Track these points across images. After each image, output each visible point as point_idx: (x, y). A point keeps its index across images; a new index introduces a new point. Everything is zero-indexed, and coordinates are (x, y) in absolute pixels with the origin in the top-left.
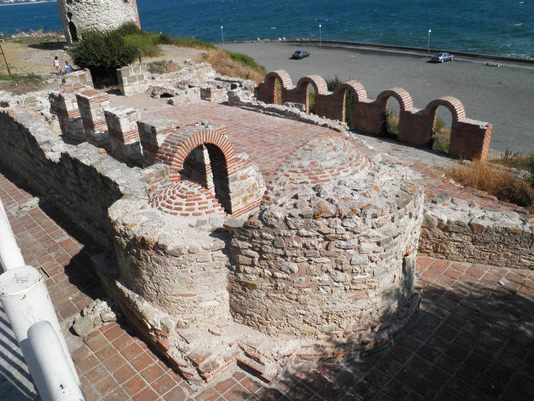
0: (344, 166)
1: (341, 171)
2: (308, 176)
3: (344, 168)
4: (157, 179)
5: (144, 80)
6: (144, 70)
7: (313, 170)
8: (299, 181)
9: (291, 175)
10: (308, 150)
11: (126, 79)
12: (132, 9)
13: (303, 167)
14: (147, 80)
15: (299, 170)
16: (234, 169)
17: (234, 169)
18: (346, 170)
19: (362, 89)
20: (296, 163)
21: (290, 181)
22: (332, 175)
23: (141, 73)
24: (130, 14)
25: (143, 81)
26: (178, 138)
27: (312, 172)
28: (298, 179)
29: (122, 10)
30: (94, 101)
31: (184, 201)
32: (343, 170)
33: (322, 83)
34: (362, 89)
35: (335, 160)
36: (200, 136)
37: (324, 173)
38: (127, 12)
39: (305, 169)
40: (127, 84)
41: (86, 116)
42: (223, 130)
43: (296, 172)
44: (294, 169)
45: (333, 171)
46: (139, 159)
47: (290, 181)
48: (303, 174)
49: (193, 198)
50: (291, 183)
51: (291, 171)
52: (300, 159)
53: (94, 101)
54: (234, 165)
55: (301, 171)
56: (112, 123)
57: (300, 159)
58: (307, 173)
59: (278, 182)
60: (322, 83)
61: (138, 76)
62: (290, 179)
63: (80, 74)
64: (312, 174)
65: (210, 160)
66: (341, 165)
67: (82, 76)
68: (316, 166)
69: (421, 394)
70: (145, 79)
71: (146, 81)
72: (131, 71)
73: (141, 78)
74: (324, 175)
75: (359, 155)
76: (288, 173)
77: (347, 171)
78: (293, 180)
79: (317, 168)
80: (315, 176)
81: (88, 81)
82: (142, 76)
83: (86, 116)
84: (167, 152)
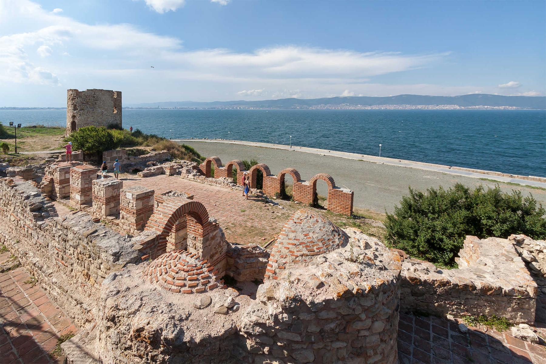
4: (148, 246)
8: (299, 254)
11: (109, 158)
12: (118, 116)
23: (121, 155)
24: (117, 119)
29: (112, 116)
38: (115, 118)
40: (109, 161)
51: (289, 244)
55: (299, 244)
62: (290, 251)
71: (124, 160)
72: (114, 154)
82: (122, 156)
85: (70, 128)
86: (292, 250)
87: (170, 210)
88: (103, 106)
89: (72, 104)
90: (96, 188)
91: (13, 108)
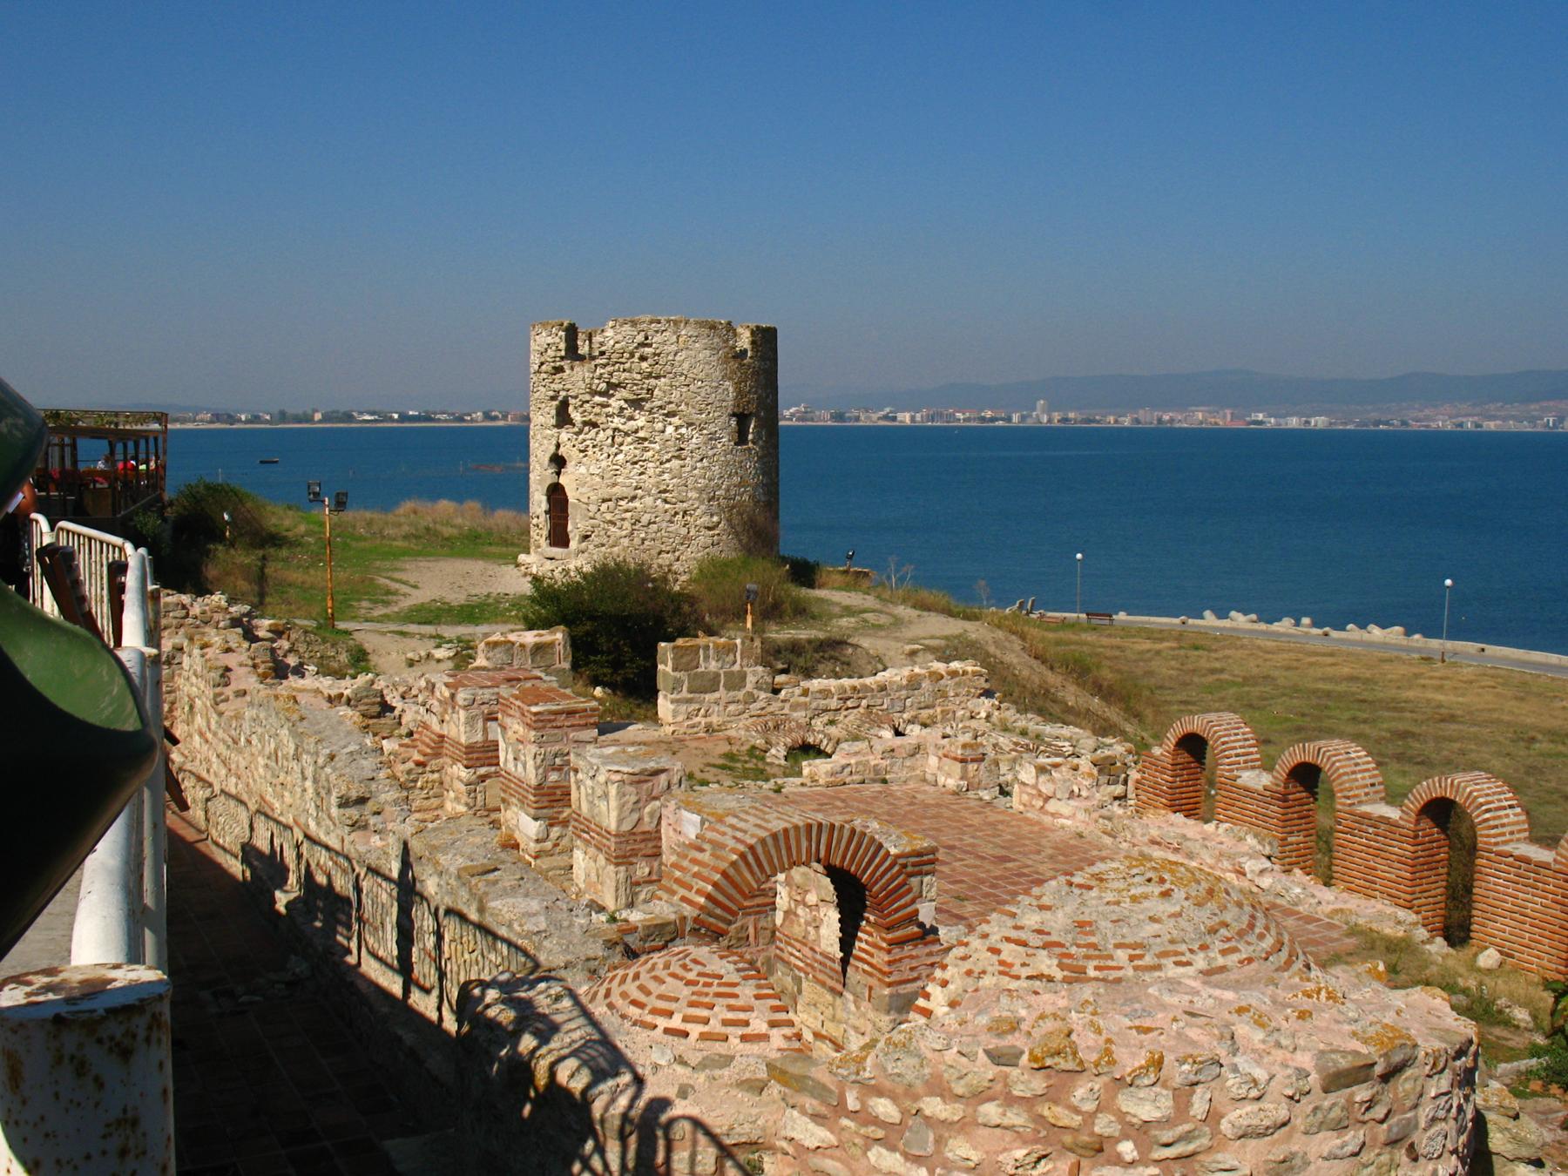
0: (1183, 948)
1: (1168, 962)
2: (1055, 962)
3: (1176, 953)
5: (744, 691)
6: (749, 658)
7: (1078, 946)
8: (1025, 972)
9: (1009, 952)
10: (1080, 886)
13: (1049, 934)
14: (755, 691)
15: (1036, 940)
16: (912, 969)
17: (912, 969)
18: (1184, 959)
19: (1511, 807)
20: (1032, 919)
21: (1001, 968)
22: (1136, 968)
23: (736, 667)
25: (740, 695)
26: (739, 835)
27: (1073, 950)
28: (1024, 965)
30: (550, 721)
31: (685, 992)
32: (1174, 959)
33: (1367, 770)
34: (1511, 807)
35: (1156, 926)
36: (809, 840)
37: (1111, 957)
39: (1054, 938)
41: (516, 766)
42: (925, 858)
43: (1024, 944)
44: (1022, 935)
45: (1141, 957)
46: (660, 949)
47: (1001, 968)
48: (1044, 953)
49: (715, 989)
50: (1001, 973)
51: (1008, 940)
52: (1048, 908)
53: (550, 721)
54: (912, 957)
56: (587, 795)
57: (1048, 908)
58: (1058, 950)
59: (967, 965)
60: (1367, 770)
61: (729, 675)
62: (1002, 963)
63: (537, 639)
64: (1070, 956)
65: (841, 930)
66: (1172, 942)
67: (539, 649)
68: (1092, 933)
69: (419, 623)
70: (749, 687)
72: (707, 658)
73: (736, 681)
74: (1110, 963)
75: (1252, 926)
76: (999, 946)
77: (1189, 964)
78: (1011, 965)
79: (1093, 939)
80: (1081, 963)
81: (557, 665)
82: (743, 677)
83: (516, 766)
84: (696, 869)
85: (542, 518)
86: (1009, 960)
87: (738, 840)
88: (683, 407)
89: (553, 398)
90: (582, 788)
91: (345, 413)
